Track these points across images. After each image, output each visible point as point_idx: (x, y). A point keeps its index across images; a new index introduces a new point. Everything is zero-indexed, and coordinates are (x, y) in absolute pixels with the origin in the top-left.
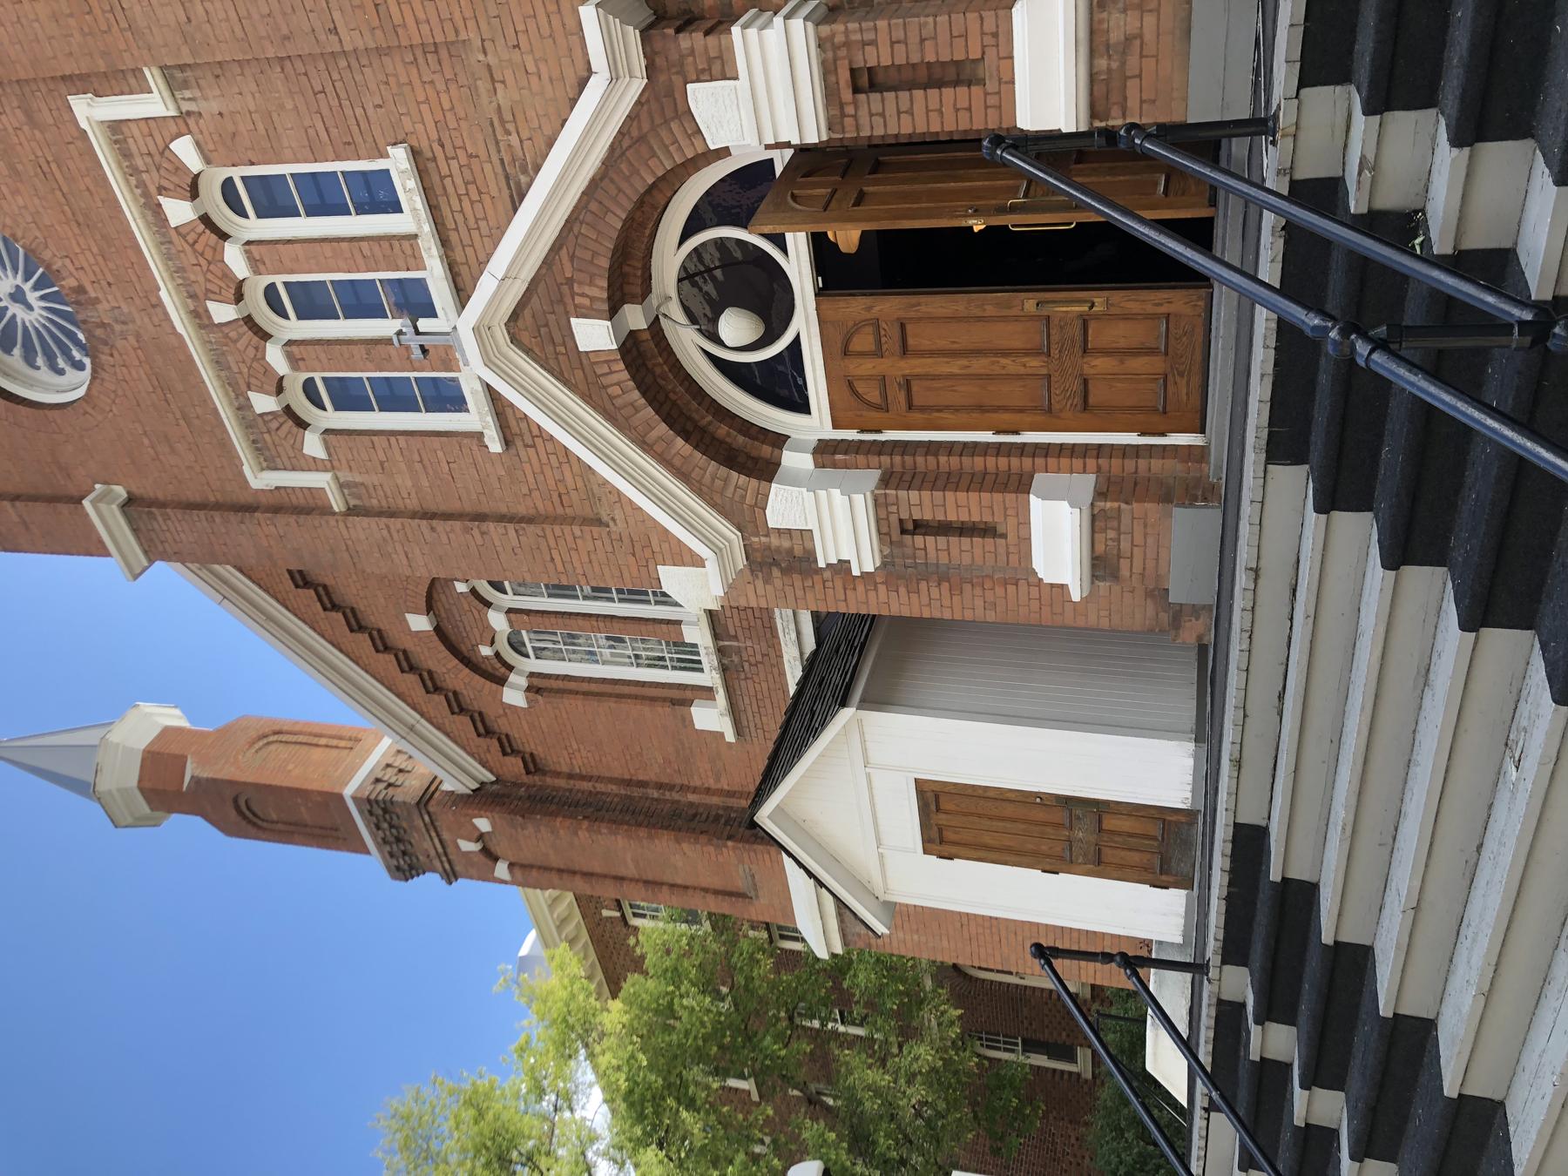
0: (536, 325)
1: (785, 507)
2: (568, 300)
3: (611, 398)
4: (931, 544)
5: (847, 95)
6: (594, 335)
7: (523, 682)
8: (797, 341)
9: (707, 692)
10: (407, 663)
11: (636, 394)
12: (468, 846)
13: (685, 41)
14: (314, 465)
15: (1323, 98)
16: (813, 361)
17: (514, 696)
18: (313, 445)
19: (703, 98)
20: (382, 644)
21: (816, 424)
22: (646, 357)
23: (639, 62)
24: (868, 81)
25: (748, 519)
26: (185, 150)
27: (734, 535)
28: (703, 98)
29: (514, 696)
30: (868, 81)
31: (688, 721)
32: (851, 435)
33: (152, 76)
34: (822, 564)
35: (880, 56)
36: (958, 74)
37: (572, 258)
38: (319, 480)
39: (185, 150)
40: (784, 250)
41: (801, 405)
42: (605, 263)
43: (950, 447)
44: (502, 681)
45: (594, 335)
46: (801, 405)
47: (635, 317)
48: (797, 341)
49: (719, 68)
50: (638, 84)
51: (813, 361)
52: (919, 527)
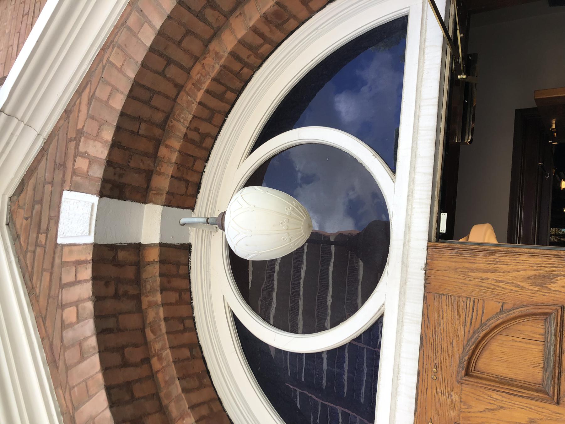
2: (69, 165)
3: (64, 326)
6: (79, 218)
16: (396, 373)
37: (91, 99)
40: (391, 163)
45: (79, 218)
47: (149, 224)
48: (373, 334)
51: (396, 373)
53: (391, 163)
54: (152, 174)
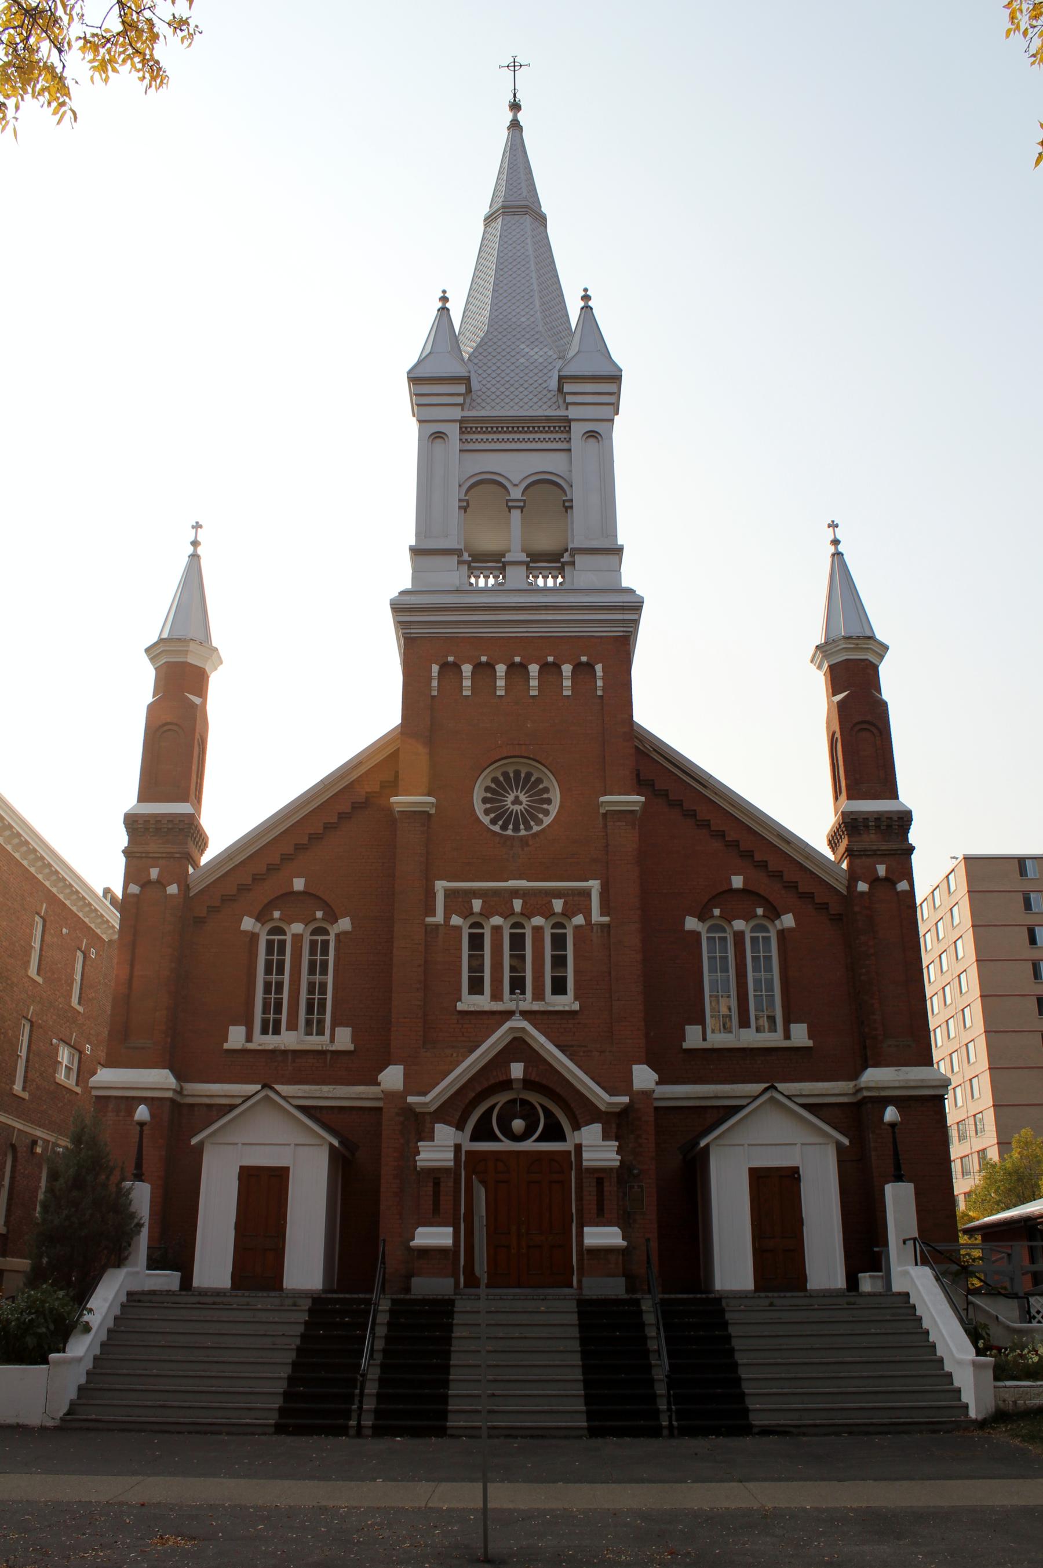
0: (518, 1047)
1: (445, 1135)
4: (429, 1189)
5: (596, 1175)
6: (517, 1070)
7: (257, 930)
8: (499, 1140)
9: (249, 1038)
10: (272, 869)
11: (493, 1081)
12: (154, 873)
13: (614, 1126)
14: (447, 918)
15: (389, 1302)
17: (248, 924)
18: (456, 920)
19: (597, 1128)
20: (286, 858)
21: (469, 1146)
22: (508, 1084)
23: (609, 1110)
24: (600, 1182)
25: (442, 1114)
26: (579, 920)
27: (432, 1109)
28: (597, 1128)
29: (248, 924)
30: (600, 1182)
31: (236, 1023)
32: (463, 1158)
33: (606, 919)
34: (419, 1144)
35: (606, 1184)
36: (600, 1210)
38: (439, 918)
39: (579, 920)
40: (535, 1141)
41: (474, 1138)
42: (544, 1082)
43: (1021, 1387)
44: (258, 919)
45: (517, 1070)
46: (474, 1138)
49: (606, 1137)
50: (603, 1108)
52: (437, 1184)
53: (535, 1141)
54: (590, 1302)
